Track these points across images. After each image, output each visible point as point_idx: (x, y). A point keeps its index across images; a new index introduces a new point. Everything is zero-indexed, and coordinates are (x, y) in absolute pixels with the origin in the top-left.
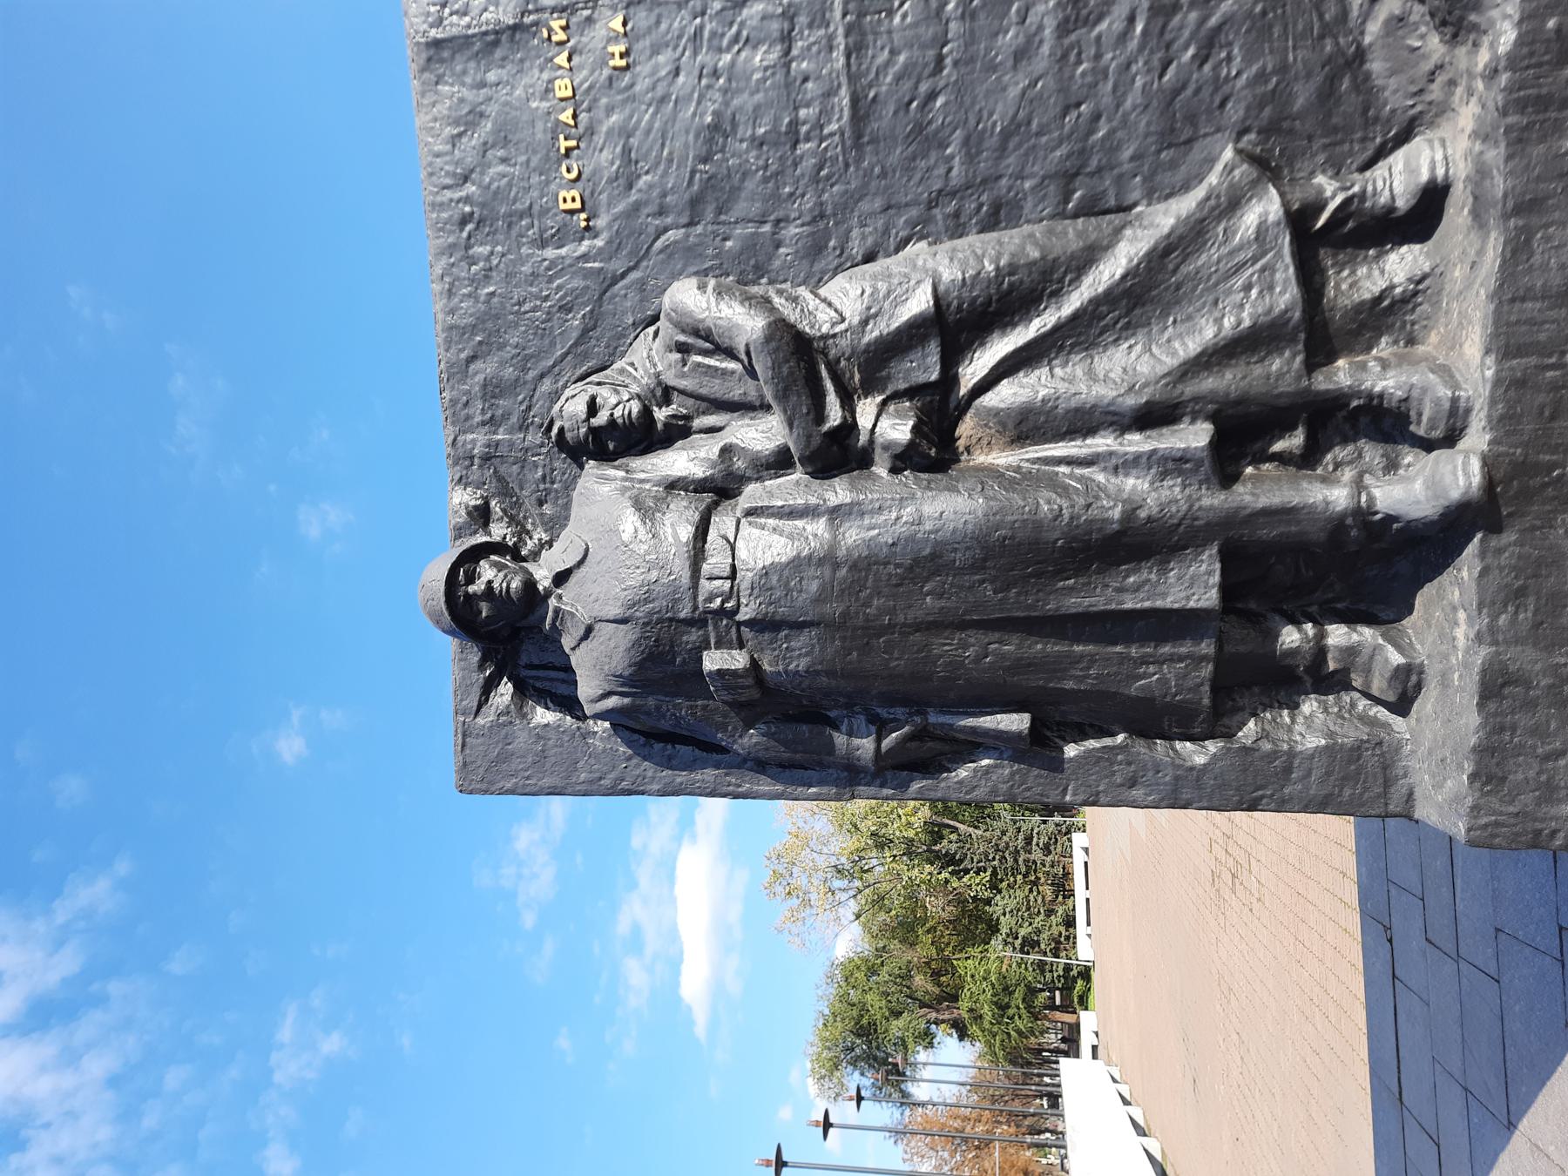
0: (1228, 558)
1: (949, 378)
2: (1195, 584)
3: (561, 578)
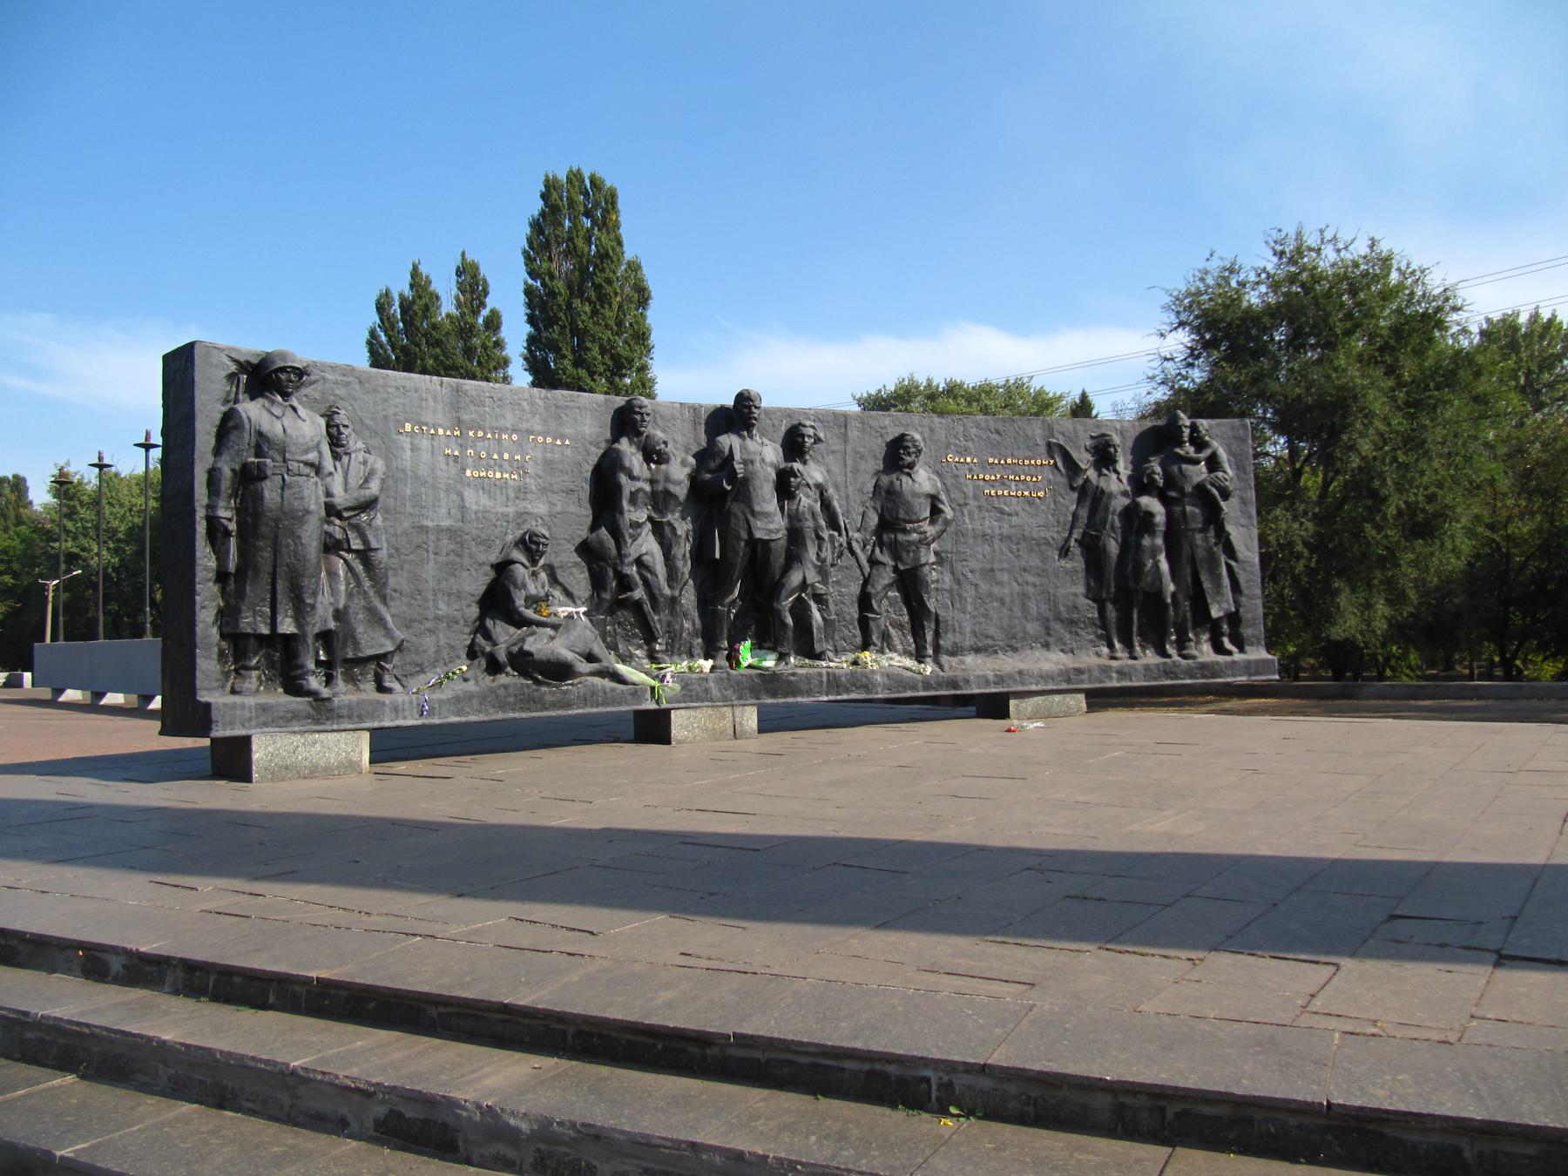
0: (293, 636)
1: (349, 550)
2: (287, 626)
3: (295, 409)
